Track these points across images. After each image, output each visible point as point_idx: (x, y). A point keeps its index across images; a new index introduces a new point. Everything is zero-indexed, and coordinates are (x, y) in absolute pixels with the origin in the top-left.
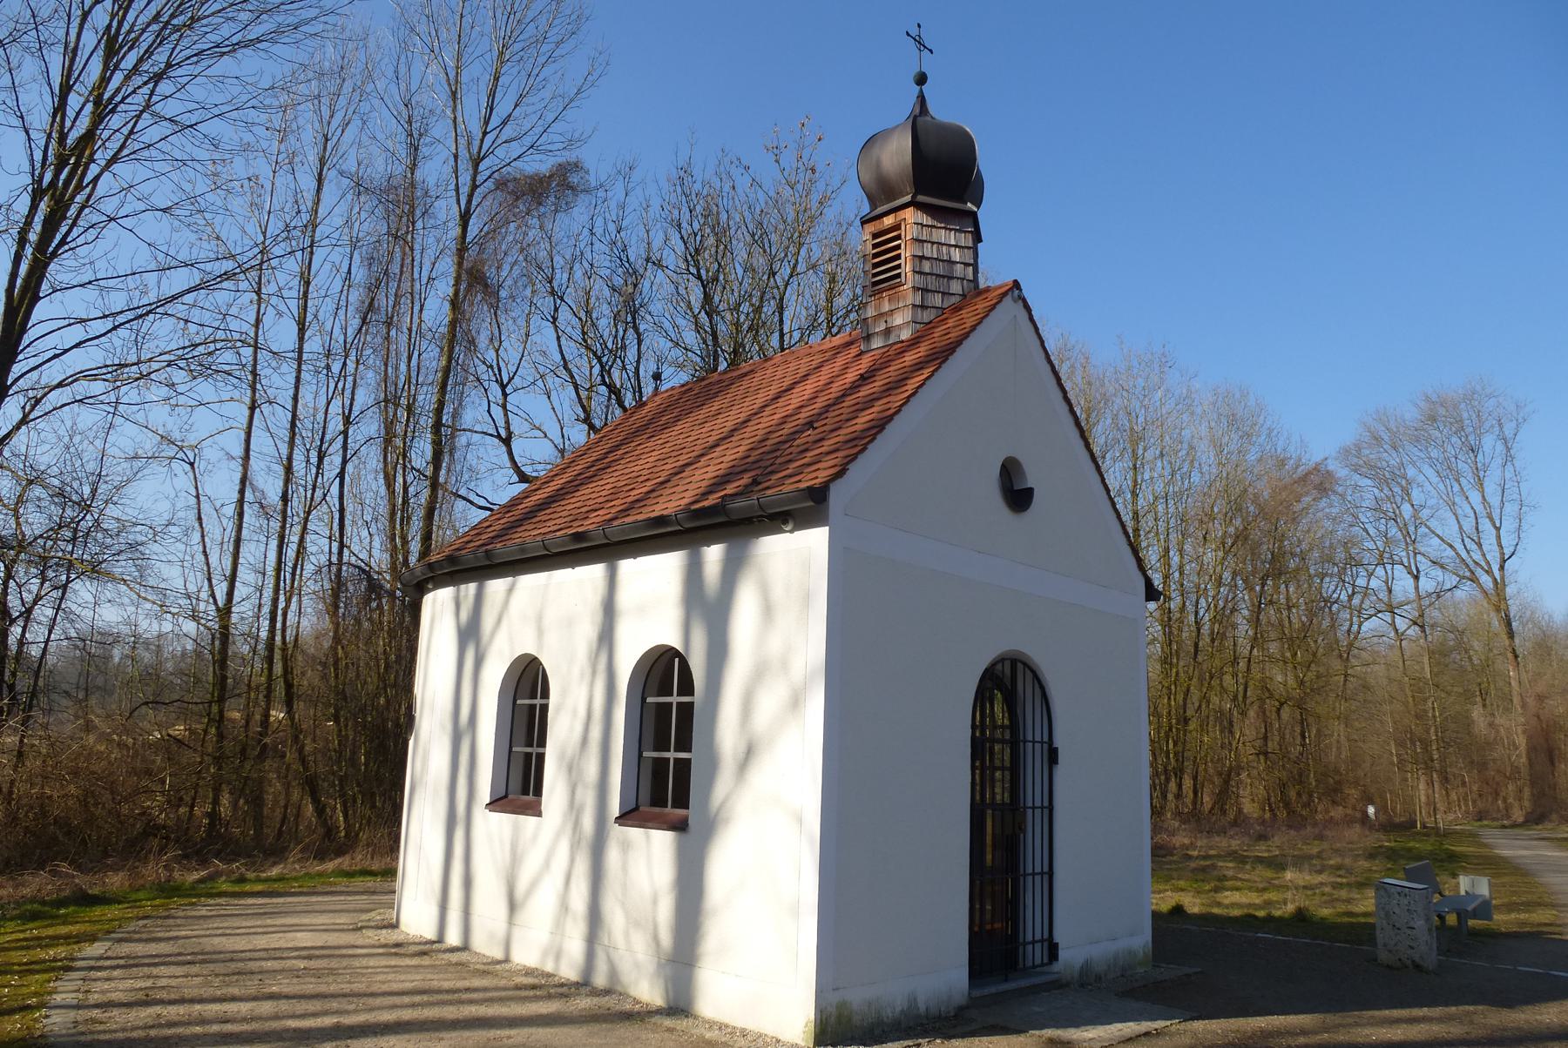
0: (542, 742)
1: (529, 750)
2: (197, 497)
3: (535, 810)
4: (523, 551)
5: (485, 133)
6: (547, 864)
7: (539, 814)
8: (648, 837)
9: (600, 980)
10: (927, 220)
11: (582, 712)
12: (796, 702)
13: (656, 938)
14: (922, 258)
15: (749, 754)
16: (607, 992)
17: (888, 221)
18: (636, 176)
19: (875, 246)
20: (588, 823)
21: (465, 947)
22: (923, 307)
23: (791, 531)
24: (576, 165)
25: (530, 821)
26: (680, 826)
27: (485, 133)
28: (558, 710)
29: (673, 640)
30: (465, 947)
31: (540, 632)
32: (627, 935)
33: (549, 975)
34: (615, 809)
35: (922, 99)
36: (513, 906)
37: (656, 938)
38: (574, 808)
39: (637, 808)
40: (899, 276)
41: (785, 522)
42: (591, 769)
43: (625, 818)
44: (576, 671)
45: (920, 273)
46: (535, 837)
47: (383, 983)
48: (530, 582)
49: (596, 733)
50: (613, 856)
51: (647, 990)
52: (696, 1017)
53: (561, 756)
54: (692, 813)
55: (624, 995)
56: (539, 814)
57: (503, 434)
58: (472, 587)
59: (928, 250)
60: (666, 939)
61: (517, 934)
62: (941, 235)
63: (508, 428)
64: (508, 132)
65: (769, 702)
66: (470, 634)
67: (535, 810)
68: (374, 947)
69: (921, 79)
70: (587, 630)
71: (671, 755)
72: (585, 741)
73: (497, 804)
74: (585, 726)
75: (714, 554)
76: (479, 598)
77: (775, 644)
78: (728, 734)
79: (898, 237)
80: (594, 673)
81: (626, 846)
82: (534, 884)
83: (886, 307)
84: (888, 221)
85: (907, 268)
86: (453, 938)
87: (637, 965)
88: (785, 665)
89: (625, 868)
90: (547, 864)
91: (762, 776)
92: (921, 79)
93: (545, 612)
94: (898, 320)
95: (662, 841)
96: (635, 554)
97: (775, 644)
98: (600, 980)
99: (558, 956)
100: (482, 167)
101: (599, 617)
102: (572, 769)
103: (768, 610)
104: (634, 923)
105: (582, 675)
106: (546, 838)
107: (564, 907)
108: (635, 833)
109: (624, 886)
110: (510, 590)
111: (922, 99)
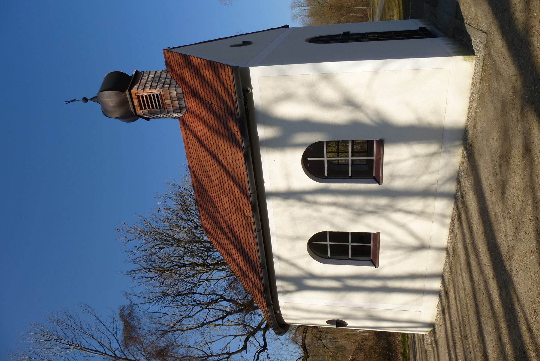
0: (347, 234)
3: (377, 236)
4: (259, 231)
5: (106, 354)
6: (402, 226)
7: (379, 233)
8: (388, 163)
9: (451, 187)
10: (137, 86)
11: (332, 209)
13: (433, 155)
14: (151, 86)
15: (350, 103)
16: (459, 182)
17: (136, 102)
18: (129, 292)
19: (145, 108)
20: (383, 201)
21: (442, 277)
22: (170, 84)
23: (252, 88)
24: (121, 310)
25: (383, 238)
26: (381, 143)
27: (106, 354)
28: (333, 225)
29: (299, 154)
30: (442, 277)
31: (298, 238)
32: (432, 173)
33: (453, 220)
34: (374, 186)
35: (92, 99)
36: (422, 247)
37: (433, 155)
38: (376, 211)
39: (371, 260)
40: (157, 95)
41: (247, 91)
42: (358, 201)
43: (378, 180)
44: (315, 214)
45: (157, 86)
46: (390, 235)
47: (465, 289)
48: (277, 247)
49: (342, 199)
50: (398, 184)
51: (430, 329)
52: (466, 127)
53: (354, 221)
54: (375, 137)
55: (459, 173)
56: (379, 233)
57: (227, 356)
58: (278, 283)
59: (149, 84)
60: (433, 148)
61: (435, 244)
62: (143, 81)
63: (225, 354)
64: (105, 342)
65: (328, 93)
66: (300, 283)
67: (377, 236)
68: (444, 319)
70: (297, 209)
71: (350, 244)
72: (346, 207)
73: (374, 263)
75: (262, 132)
76: (284, 278)
77: (301, 91)
78: (340, 116)
79: (142, 96)
80: (315, 203)
81: (392, 177)
82: (412, 234)
83: (168, 102)
84: (136, 102)
85: (154, 91)
86: (437, 285)
87: (446, 165)
88: (311, 85)
89: (402, 177)
90: (402, 226)
91: (360, 94)
92: (85, 100)
93: (289, 231)
94: (174, 94)
96: (262, 182)
97: (301, 91)
98: (451, 187)
99: (443, 216)
100: (119, 356)
101: (291, 202)
102: (360, 212)
103: (288, 97)
104: (426, 169)
105: (317, 211)
106: (390, 227)
107: (421, 214)
108: (386, 171)
109: (411, 176)
110: (280, 258)
111: (92, 99)
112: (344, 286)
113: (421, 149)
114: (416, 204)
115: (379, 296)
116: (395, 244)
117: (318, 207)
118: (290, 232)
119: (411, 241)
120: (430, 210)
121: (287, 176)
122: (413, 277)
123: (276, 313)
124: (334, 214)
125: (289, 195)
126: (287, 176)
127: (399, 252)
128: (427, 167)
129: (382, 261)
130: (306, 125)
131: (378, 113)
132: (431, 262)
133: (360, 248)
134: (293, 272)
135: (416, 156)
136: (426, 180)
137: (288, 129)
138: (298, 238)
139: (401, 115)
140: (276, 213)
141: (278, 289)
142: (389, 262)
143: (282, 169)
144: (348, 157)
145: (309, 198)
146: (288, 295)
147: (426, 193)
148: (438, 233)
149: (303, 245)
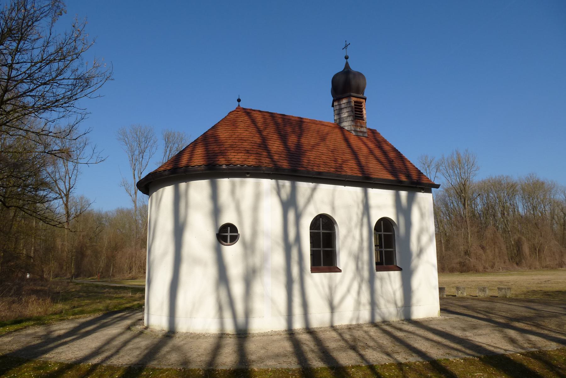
1: (319, 249)
2: (69, 79)
6: (348, 291)
12: (431, 240)
13: (396, 304)
20: (366, 274)
30: (171, 333)
32: (385, 305)
35: (347, 63)
36: (332, 308)
37: (396, 304)
46: (341, 282)
48: (325, 189)
50: (378, 284)
53: (350, 253)
60: (400, 303)
65: (425, 239)
69: (347, 58)
70: (356, 211)
72: (361, 249)
73: (314, 270)
74: (352, 242)
76: (294, 190)
80: (362, 225)
81: (382, 279)
82: (343, 299)
87: (390, 314)
89: (382, 287)
90: (348, 291)
92: (347, 58)
95: (395, 276)
99: (358, 319)
101: (361, 207)
107: (358, 303)
108: (384, 274)
110: (314, 190)
111: (347, 63)
112: (289, 246)
113: (399, 295)
114: (365, 297)
115: (282, 279)
116: (334, 286)
117: (359, 227)
118: (337, 203)
119: (336, 300)
120: (362, 308)
121: (379, 207)
122: (305, 305)
123: (248, 173)
124: (354, 238)
125: (366, 208)
126: (379, 207)
127: (327, 290)
128: (388, 301)
129: (317, 275)
130: (408, 224)
131: (416, 267)
132: (319, 317)
133: (324, 255)
134: (301, 200)
135: (394, 294)
136: (382, 302)
137: (404, 211)
138: (333, 208)
139: (417, 281)
140: (350, 194)
141: (281, 182)
142: (317, 282)
143: (383, 203)
144: (388, 246)
145: (365, 220)
146: (275, 193)
147: (373, 304)
148: (346, 317)
149: (327, 211)
